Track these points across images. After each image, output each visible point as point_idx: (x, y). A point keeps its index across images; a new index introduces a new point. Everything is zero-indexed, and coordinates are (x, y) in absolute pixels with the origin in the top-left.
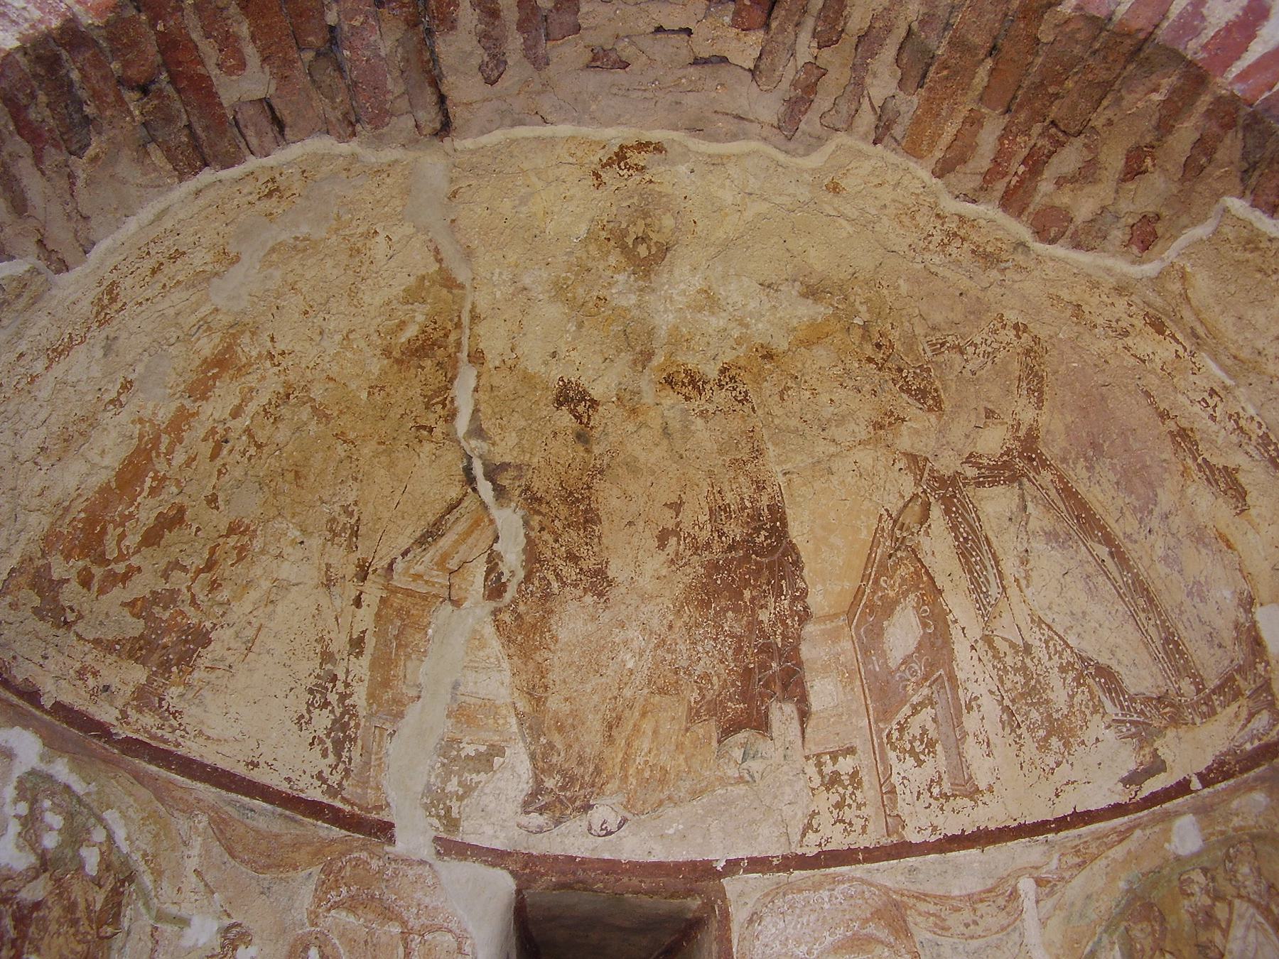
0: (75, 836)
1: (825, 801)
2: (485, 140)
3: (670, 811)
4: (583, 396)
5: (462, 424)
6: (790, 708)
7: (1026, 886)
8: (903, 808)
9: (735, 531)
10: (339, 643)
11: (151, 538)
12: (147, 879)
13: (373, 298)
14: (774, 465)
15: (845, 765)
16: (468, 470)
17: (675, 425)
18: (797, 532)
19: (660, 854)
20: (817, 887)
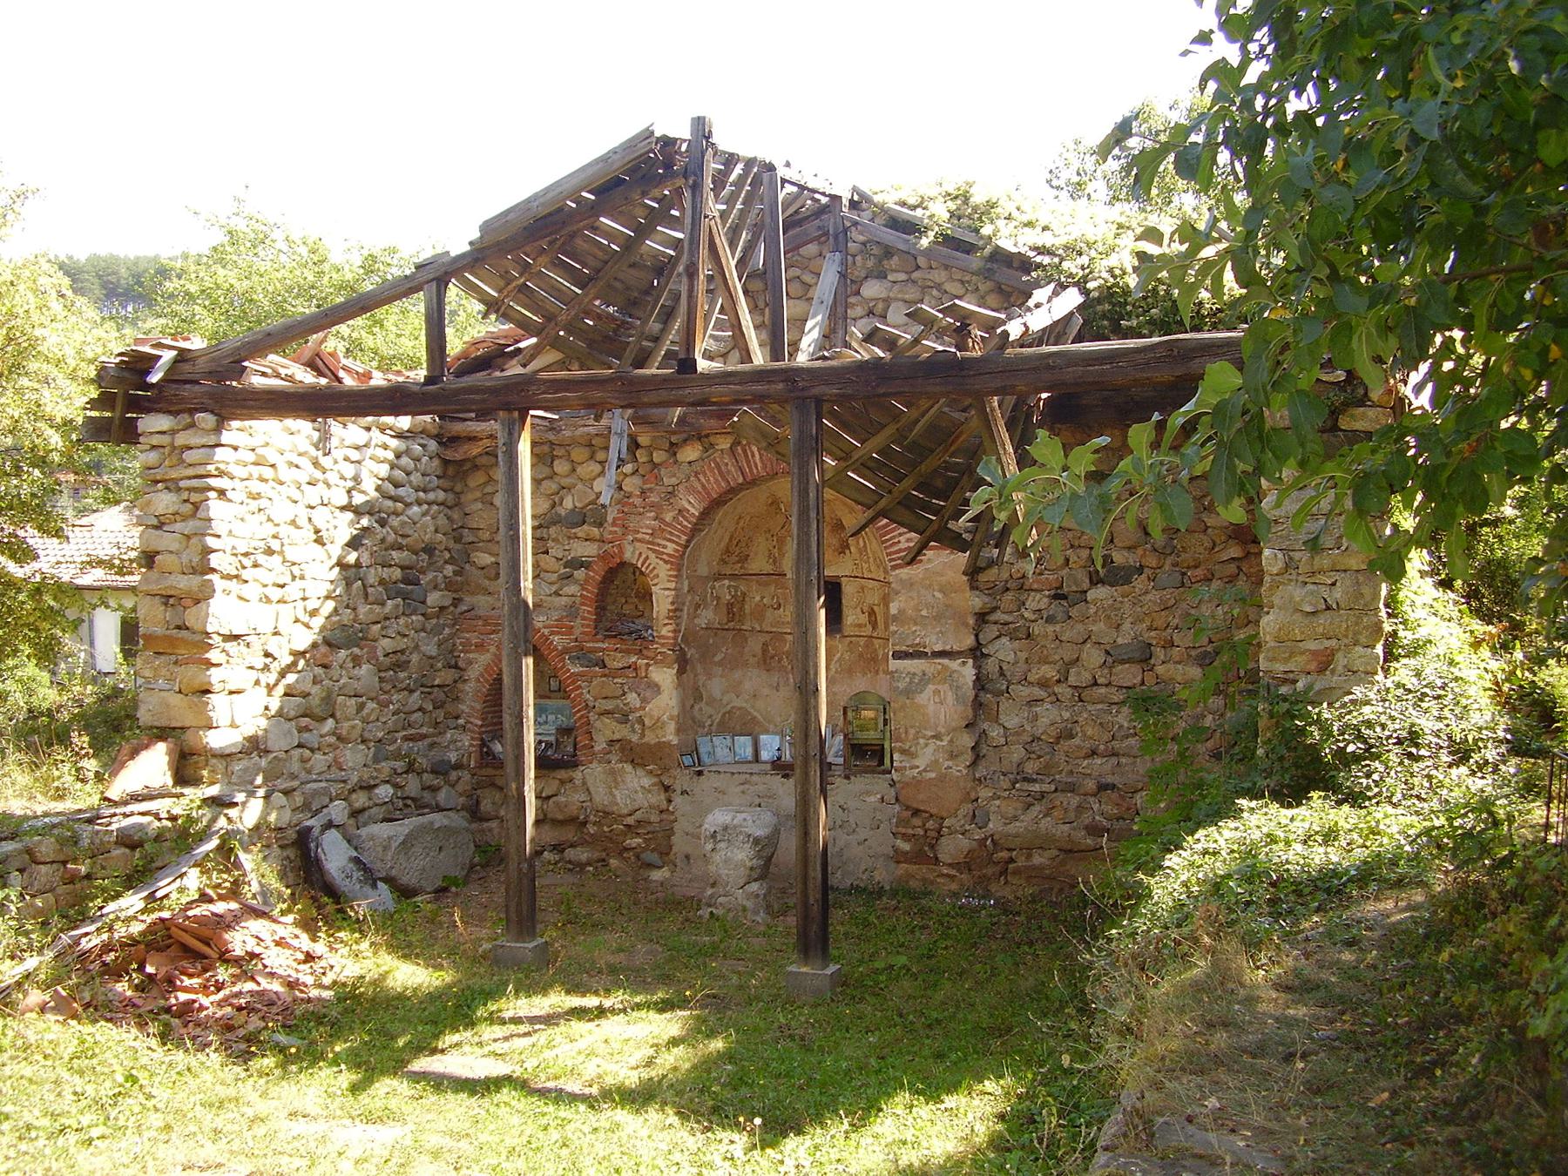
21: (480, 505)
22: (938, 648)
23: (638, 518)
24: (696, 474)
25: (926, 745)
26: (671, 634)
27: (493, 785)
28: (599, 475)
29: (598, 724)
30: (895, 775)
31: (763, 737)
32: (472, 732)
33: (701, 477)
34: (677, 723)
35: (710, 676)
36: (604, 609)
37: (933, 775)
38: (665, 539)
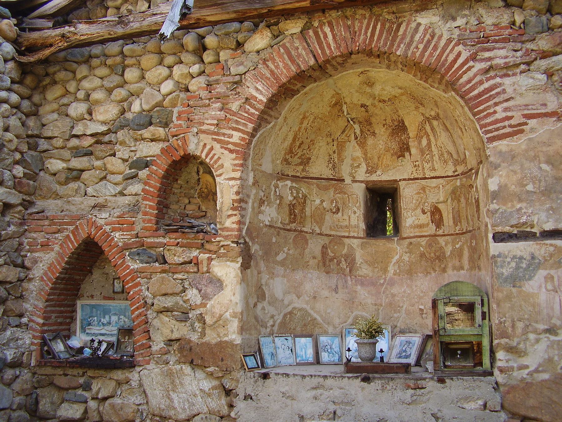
0: (298, 193)
1: (414, 169)
2: (338, 76)
3: (390, 171)
4: (365, 105)
5: (345, 113)
6: (408, 153)
7: (441, 186)
8: (425, 171)
9: (396, 123)
10: (331, 152)
11: (299, 147)
12: (309, 196)
13: (326, 100)
14: (401, 112)
15: (417, 163)
16: (348, 120)
17: (383, 107)
18: (406, 124)
19: (388, 179)
20: (413, 184)
21: (55, 116)
22: (549, 226)
23: (203, 110)
24: (265, 61)
25: (537, 341)
26: (235, 226)
27: (52, 384)
28: (167, 79)
29: (156, 323)
30: (498, 376)
31: (323, 339)
32: (34, 330)
33: (270, 64)
34: (241, 320)
35: (272, 275)
36: (167, 207)
38: (230, 128)
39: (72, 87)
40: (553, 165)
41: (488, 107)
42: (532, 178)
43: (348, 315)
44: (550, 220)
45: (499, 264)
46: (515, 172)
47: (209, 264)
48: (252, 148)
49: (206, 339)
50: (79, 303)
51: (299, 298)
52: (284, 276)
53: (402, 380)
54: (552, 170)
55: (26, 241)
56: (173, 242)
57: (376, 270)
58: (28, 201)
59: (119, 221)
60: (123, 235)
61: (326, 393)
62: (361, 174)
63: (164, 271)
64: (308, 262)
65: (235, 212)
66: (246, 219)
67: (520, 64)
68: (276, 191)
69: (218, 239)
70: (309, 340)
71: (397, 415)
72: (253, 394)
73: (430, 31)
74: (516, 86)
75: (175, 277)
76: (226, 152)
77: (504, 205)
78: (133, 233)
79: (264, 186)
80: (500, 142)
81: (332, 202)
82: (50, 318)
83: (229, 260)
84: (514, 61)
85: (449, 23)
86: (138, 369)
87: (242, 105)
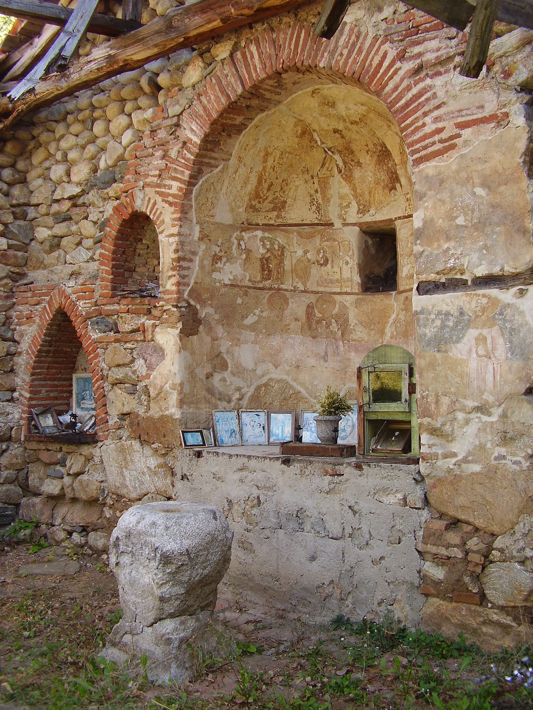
0: (272, 244)
2: (288, 100)
3: (384, 209)
4: (338, 130)
5: (319, 143)
9: (379, 148)
10: (313, 192)
11: (269, 190)
12: (287, 247)
15: (408, 196)
16: (325, 150)
17: (358, 130)
18: (389, 147)
22: (481, 271)
23: (147, 160)
25: (467, 422)
28: (128, 128)
29: (111, 396)
34: (180, 393)
35: (237, 342)
37: (476, 468)
39: (52, 148)
40: (489, 187)
41: (415, 119)
42: (463, 208)
43: (340, 387)
44: (484, 262)
45: (421, 322)
46: (443, 202)
47: (153, 331)
48: (193, 198)
49: (151, 413)
50: (74, 376)
51: (276, 367)
52: (255, 342)
53: (320, 464)
54: (488, 195)
55: (15, 314)
56: (125, 309)
57: (373, 333)
58: (18, 274)
59: (82, 289)
60: (85, 303)
61: (251, 476)
62: (353, 216)
63: (117, 341)
64: (288, 325)
65: (174, 273)
66: (190, 279)
67: (453, 57)
68: (239, 245)
69: (161, 303)
70: (289, 416)
71: (315, 505)
72: (188, 474)
73: (356, 30)
74: (448, 86)
75: (125, 347)
76: (167, 206)
77: (429, 246)
78: (93, 300)
79: (220, 240)
80: (428, 164)
81: (318, 252)
82: (40, 392)
83: (169, 327)
84: (447, 53)
85: (375, 16)
86: (100, 444)
87: (180, 150)
